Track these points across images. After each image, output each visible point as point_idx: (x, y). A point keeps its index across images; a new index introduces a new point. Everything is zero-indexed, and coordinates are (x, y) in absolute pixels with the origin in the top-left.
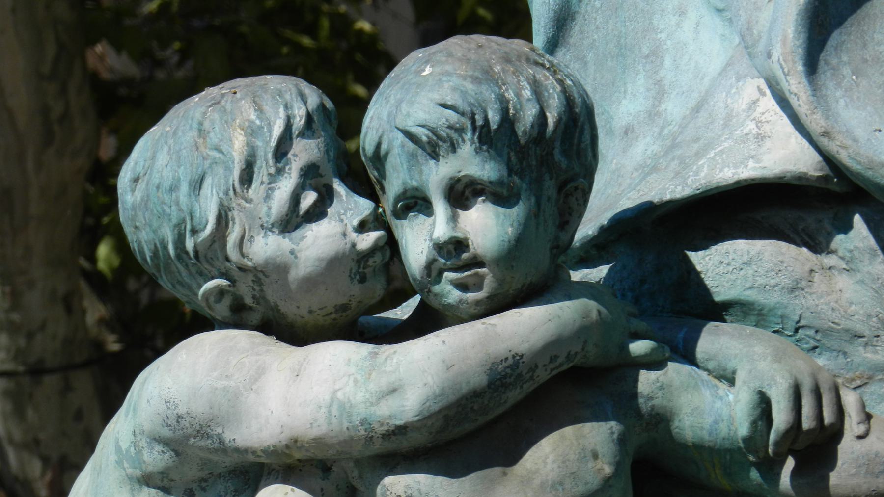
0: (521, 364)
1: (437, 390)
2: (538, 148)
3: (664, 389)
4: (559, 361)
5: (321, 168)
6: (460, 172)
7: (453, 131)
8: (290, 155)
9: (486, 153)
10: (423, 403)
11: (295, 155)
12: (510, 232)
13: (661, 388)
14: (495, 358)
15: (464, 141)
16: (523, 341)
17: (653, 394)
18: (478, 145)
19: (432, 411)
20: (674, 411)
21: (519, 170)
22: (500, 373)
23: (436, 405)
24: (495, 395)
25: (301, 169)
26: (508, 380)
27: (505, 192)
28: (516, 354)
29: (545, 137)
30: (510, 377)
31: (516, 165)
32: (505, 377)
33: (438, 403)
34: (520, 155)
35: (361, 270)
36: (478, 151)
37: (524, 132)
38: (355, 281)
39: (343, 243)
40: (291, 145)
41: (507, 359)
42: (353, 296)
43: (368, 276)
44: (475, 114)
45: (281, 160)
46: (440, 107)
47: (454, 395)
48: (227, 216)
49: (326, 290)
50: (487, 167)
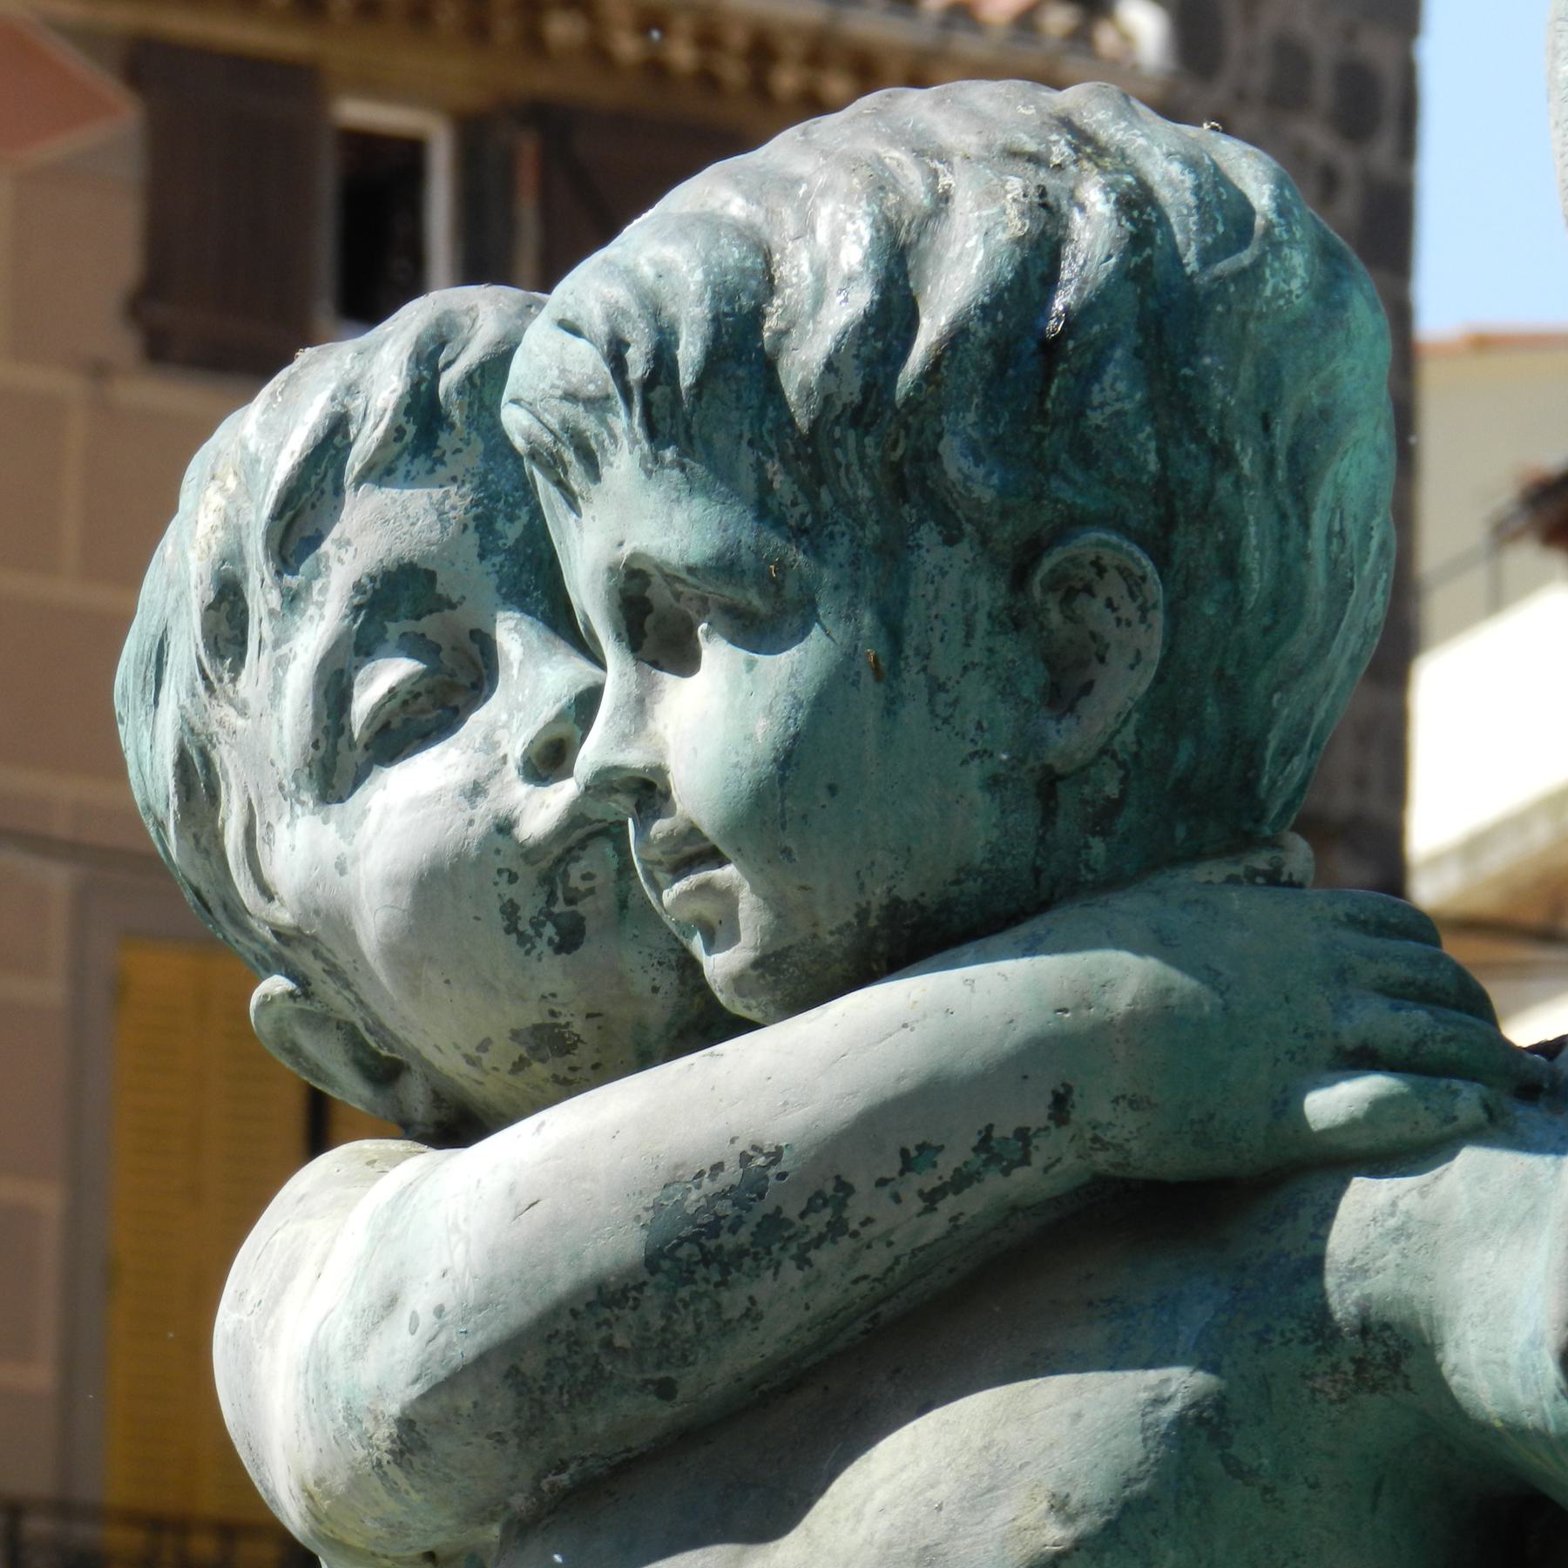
0: (772, 1181)
1: (472, 1290)
2: (869, 441)
3: (1409, 1236)
4: (946, 1165)
5: (440, 578)
6: (621, 544)
7: (581, 408)
8: (327, 546)
9: (676, 473)
10: (427, 1338)
11: (344, 543)
12: (760, 733)
13: (1401, 1233)
14: (677, 1167)
15: (613, 436)
16: (786, 1103)
17: (1366, 1259)
18: (646, 447)
19: (454, 1363)
20: (1437, 1312)
21: (809, 520)
22: (691, 1219)
23: (468, 1343)
24: (684, 1293)
25: (358, 587)
26: (727, 1241)
27: (754, 600)
28: (754, 1148)
29: (891, 402)
30: (733, 1230)
31: (794, 504)
32: (713, 1229)
33: (475, 1332)
34: (805, 471)
35: (559, 907)
36: (652, 466)
37: (806, 392)
38: (542, 946)
39: (460, 820)
40: (337, 508)
41: (718, 1167)
42: (554, 995)
43: (591, 926)
44: (628, 345)
45: (300, 561)
46: (561, 331)
47: (528, 1303)
48: (208, 763)
49: (447, 982)
50: (680, 517)
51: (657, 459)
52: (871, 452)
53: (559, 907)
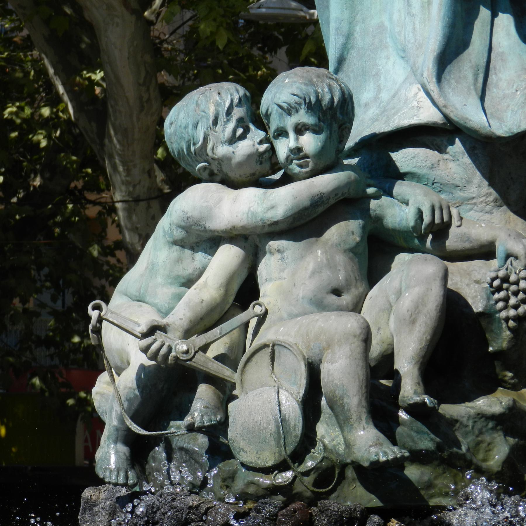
8: (232, 114)
13: (379, 207)
15: (301, 108)
25: (237, 120)
26: (319, 203)
27: (317, 129)
32: (317, 202)
35: (260, 159)
37: (325, 105)
38: (258, 164)
41: (318, 195)
50: (310, 119)
51: (308, 112)
52: (331, 113)
53: (260, 159)
